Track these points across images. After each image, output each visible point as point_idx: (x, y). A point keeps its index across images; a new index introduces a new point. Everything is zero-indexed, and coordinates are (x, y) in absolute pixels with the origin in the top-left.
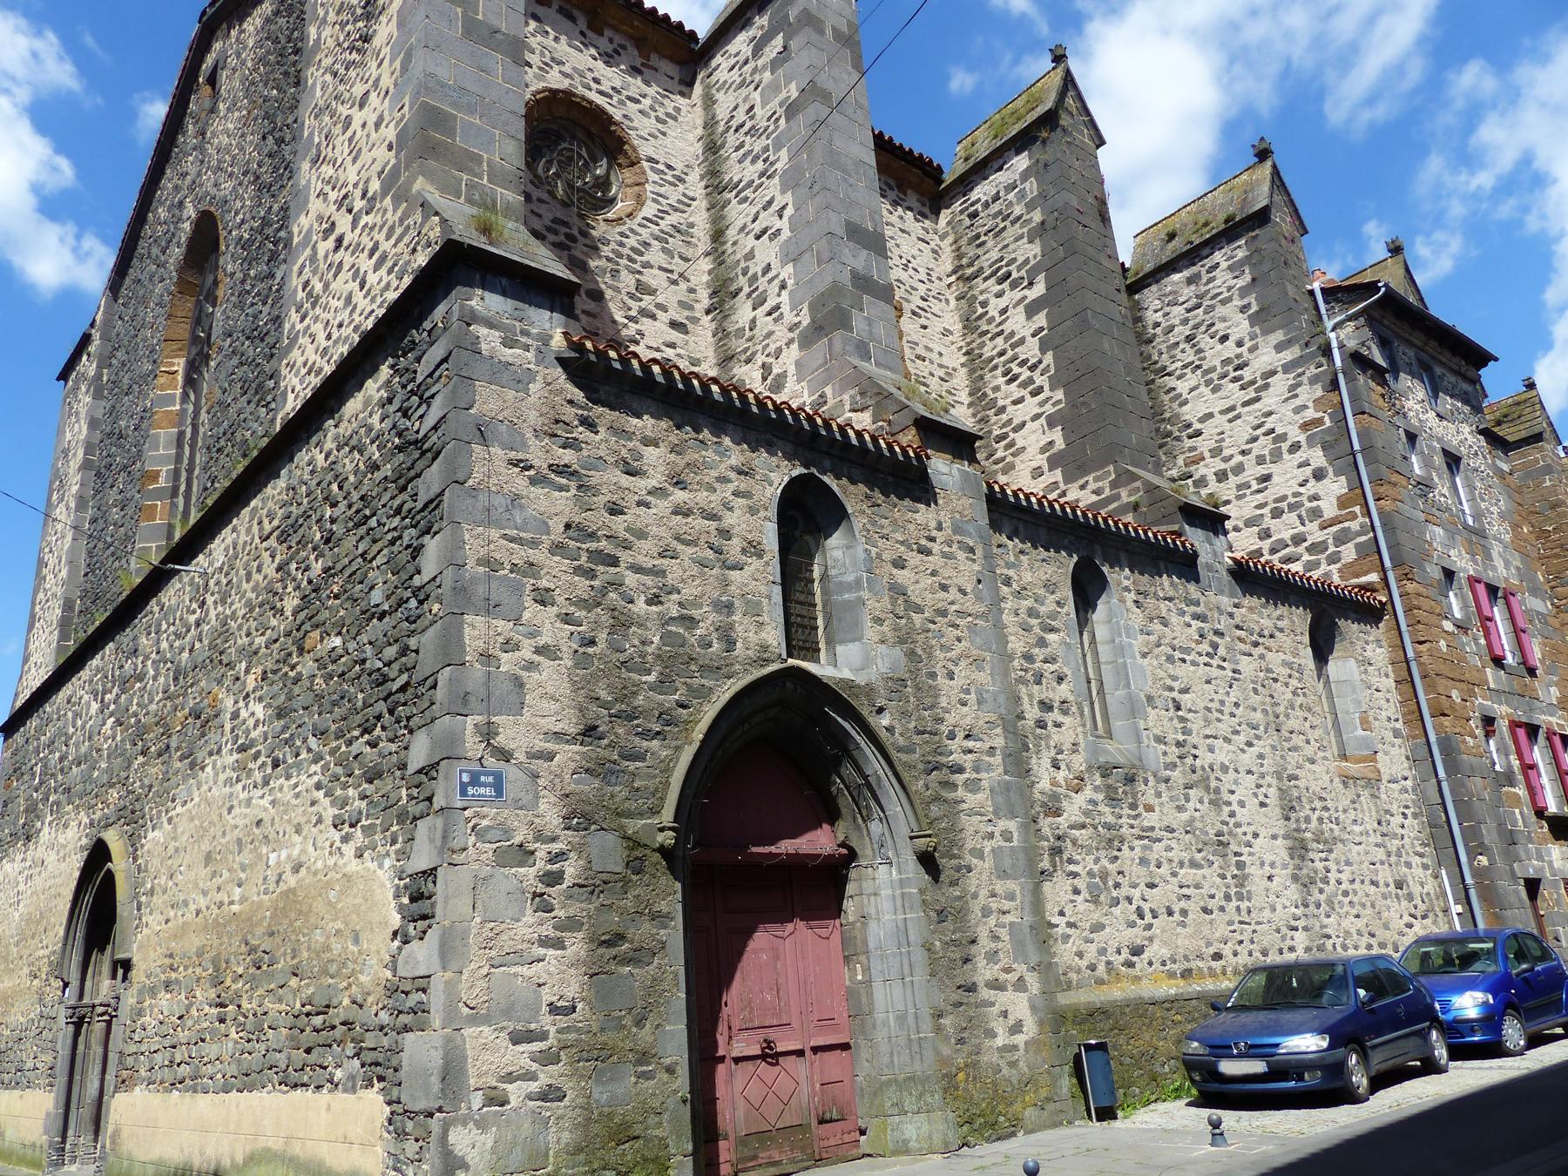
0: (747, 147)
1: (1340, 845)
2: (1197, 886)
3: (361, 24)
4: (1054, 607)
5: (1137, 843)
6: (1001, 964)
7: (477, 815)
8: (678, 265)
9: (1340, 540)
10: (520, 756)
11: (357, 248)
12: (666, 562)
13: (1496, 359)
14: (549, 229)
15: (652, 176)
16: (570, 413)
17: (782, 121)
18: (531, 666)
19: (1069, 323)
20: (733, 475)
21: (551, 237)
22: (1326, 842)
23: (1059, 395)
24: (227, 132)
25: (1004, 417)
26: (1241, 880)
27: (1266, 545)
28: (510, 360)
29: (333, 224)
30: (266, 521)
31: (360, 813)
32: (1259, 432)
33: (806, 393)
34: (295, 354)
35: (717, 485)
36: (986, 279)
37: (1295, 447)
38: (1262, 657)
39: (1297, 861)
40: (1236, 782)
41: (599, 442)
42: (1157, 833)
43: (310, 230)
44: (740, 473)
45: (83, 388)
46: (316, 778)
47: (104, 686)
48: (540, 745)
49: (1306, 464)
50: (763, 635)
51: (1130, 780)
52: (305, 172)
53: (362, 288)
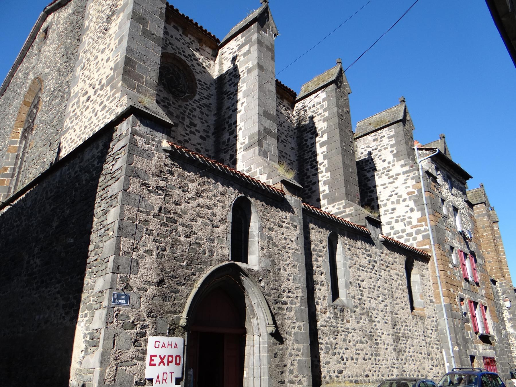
0: (233, 81)
1: (410, 339)
2: (362, 350)
6: (294, 374)
9: (417, 233)
11: (95, 102)
12: (193, 223)
13: (472, 178)
14: (162, 100)
15: (199, 86)
16: (165, 169)
17: (246, 74)
18: (142, 257)
19: (334, 151)
20: (219, 195)
21: (162, 103)
22: (406, 337)
23: (328, 174)
24: (49, 51)
25: (309, 180)
26: (377, 349)
27: (392, 232)
28: (147, 149)
30: (49, 193)
32: (393, 193)
35: (213, 198)
36: (307, 133)
37: (405, 200)
38: (389, 271)
39: (396, 344)
40: (377, 314)
41: (174, 180)
42: (350, 330)
46: (57, 289)
48: (143, 286)
49: (408, 206)
50: (223, 251)
51: (342, 311)
52: (78, 71)
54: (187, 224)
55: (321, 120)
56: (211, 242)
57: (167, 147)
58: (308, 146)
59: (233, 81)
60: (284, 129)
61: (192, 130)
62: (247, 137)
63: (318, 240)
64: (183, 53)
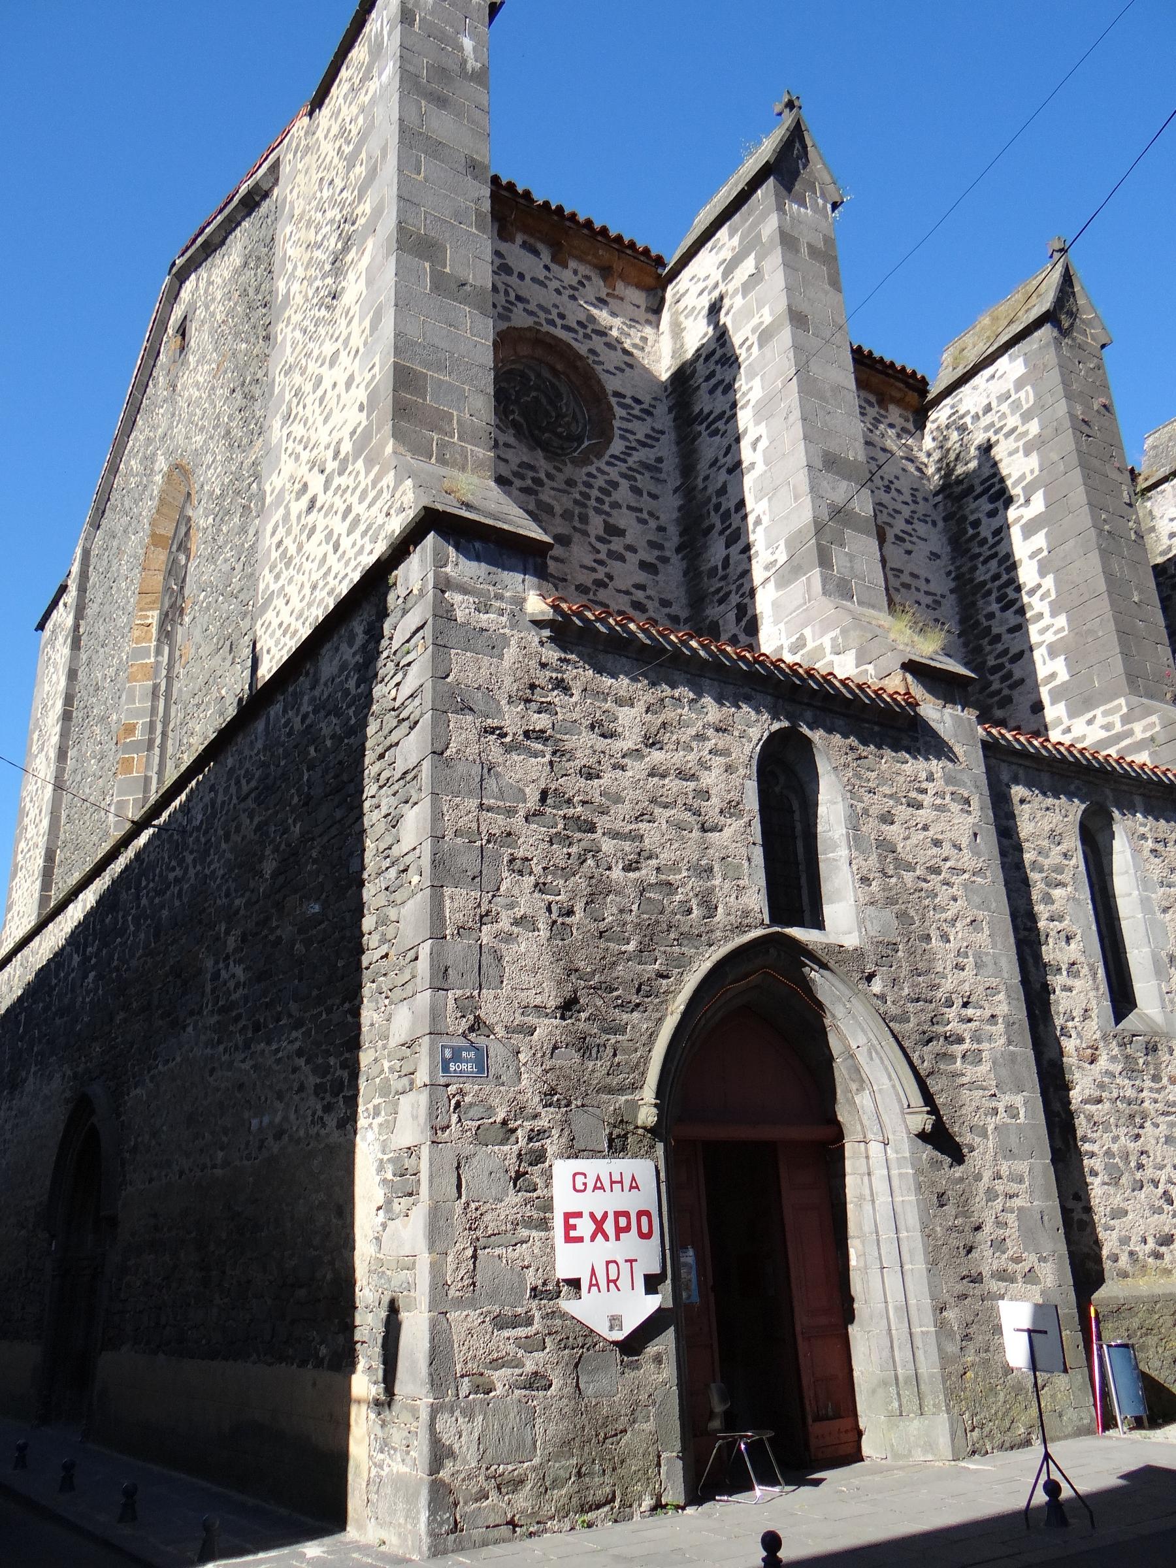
0: (718, 377)
3: (329, 281)
4: (1059, 859)
5: (1161, 1119)
6: (1010, 1253)
7: (461, 1092)
8: (646, 502)
10: (500, 1031)
12: (643, 826)
14: (515, 474)
16: (542, 677)
17: (755, 349)
18: (509, 938)
19: (1071, 543)
20: (710, 732)
21: (518, 483)
23: (1062, 621)
24: (197, 385)
25: (1000, 647)
28: (484, 625)
29: (305, 485)
30: (244, 782)
31: (342, 1082)
33: (783, 634)
34: (270, 615)
35: (694, 744)
36: (976, 498)
43: (283, 490)
44: (717, 730)
45: (61, 639)
46: (297, 1045)
47: (86, 940)
50: (744, 899)
51: (1151, 1049)
52: (276, 431)
53: (336, 551)
54: (627, 830)
55: (1016, 451)
56: (704, 875)
57: (543, 613)
58: (984, 541)
59: (718, 377)
60: (901, 498)
61: (613, 547)
62: (782, 543)
63: (1046, 834)
64: (559, 322)
